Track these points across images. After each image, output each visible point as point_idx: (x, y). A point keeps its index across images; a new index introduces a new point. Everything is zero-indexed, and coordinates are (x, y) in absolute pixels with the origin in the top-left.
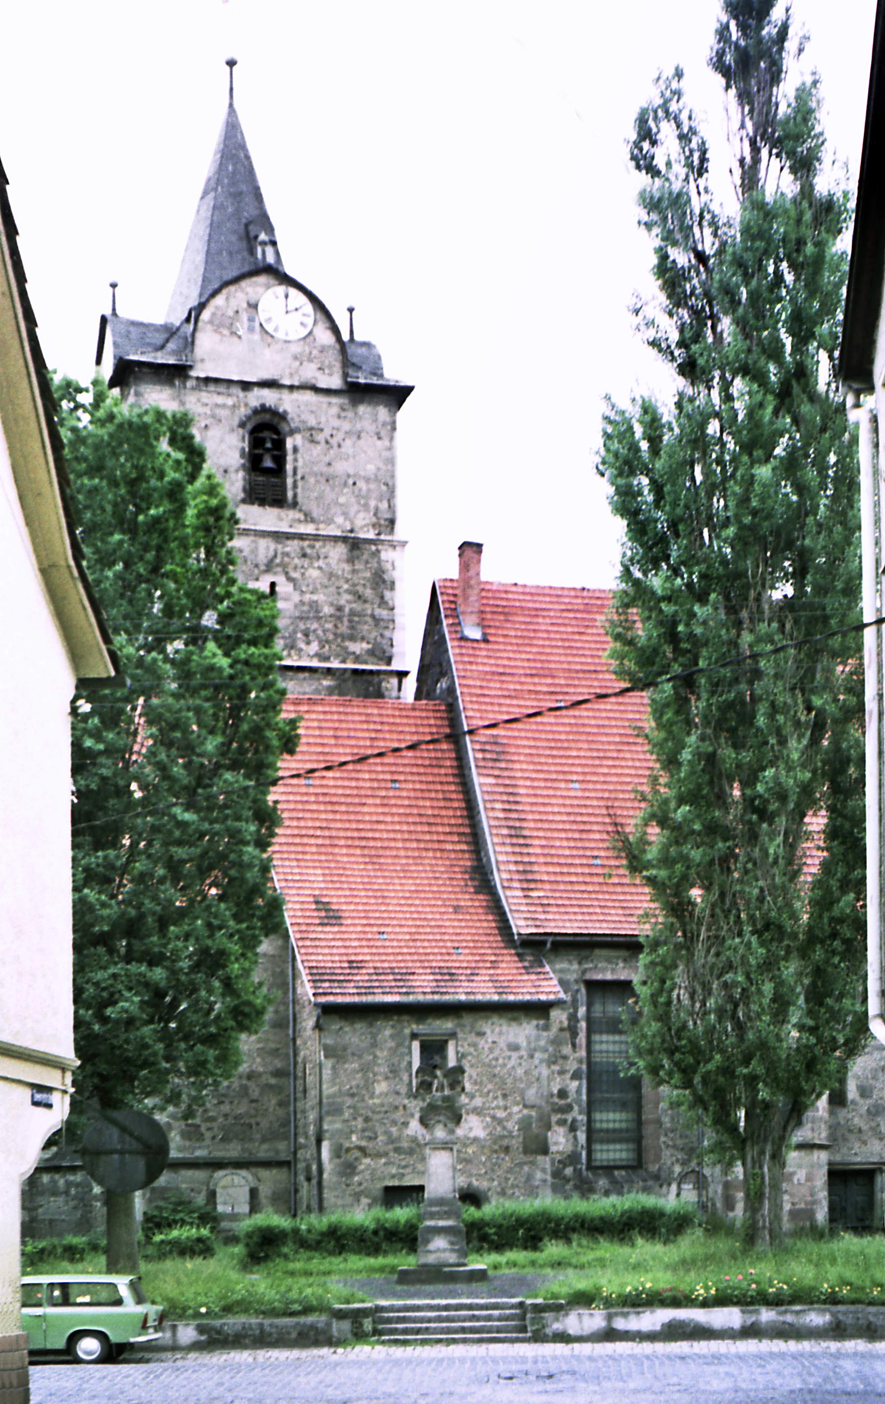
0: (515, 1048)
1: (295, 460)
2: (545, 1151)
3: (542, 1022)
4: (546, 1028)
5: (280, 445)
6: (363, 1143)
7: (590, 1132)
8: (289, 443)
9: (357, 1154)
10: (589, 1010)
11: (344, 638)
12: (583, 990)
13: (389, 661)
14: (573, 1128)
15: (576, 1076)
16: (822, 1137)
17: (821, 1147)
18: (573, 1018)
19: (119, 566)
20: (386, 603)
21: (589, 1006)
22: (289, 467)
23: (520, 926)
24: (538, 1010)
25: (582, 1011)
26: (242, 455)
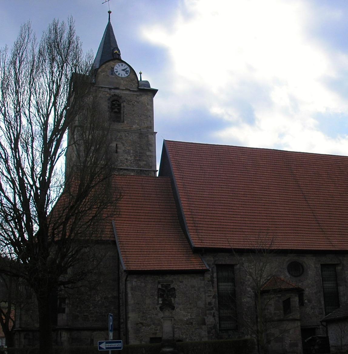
0: (193, 287)
1: (124, 109)
2: (204, 323)
3: (202, 278)
4: (204, 280)
5: (119, 105)
6: (142, 321)
7: (220, 317)
8: (122, 105)
9: (140, 325)
10: (217, 275)
11: (137, 160)
12: (215, 268)
13: (151, 167)
14: (214, 316)
15: (214, 297)
16: (298, 316)
17: (297, 320)
18: (212, 277)
19: (76, 171)
20: (150, 150)
21: (217, 273)
22: (122, 112)
23: (196, 244)
24: (202, 273)
25: (215, 275)
26: (108, 108)
